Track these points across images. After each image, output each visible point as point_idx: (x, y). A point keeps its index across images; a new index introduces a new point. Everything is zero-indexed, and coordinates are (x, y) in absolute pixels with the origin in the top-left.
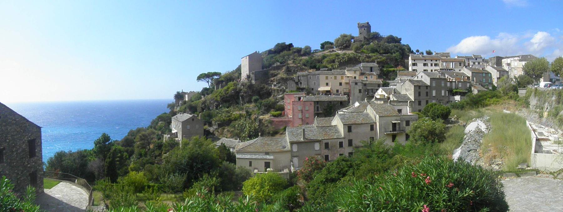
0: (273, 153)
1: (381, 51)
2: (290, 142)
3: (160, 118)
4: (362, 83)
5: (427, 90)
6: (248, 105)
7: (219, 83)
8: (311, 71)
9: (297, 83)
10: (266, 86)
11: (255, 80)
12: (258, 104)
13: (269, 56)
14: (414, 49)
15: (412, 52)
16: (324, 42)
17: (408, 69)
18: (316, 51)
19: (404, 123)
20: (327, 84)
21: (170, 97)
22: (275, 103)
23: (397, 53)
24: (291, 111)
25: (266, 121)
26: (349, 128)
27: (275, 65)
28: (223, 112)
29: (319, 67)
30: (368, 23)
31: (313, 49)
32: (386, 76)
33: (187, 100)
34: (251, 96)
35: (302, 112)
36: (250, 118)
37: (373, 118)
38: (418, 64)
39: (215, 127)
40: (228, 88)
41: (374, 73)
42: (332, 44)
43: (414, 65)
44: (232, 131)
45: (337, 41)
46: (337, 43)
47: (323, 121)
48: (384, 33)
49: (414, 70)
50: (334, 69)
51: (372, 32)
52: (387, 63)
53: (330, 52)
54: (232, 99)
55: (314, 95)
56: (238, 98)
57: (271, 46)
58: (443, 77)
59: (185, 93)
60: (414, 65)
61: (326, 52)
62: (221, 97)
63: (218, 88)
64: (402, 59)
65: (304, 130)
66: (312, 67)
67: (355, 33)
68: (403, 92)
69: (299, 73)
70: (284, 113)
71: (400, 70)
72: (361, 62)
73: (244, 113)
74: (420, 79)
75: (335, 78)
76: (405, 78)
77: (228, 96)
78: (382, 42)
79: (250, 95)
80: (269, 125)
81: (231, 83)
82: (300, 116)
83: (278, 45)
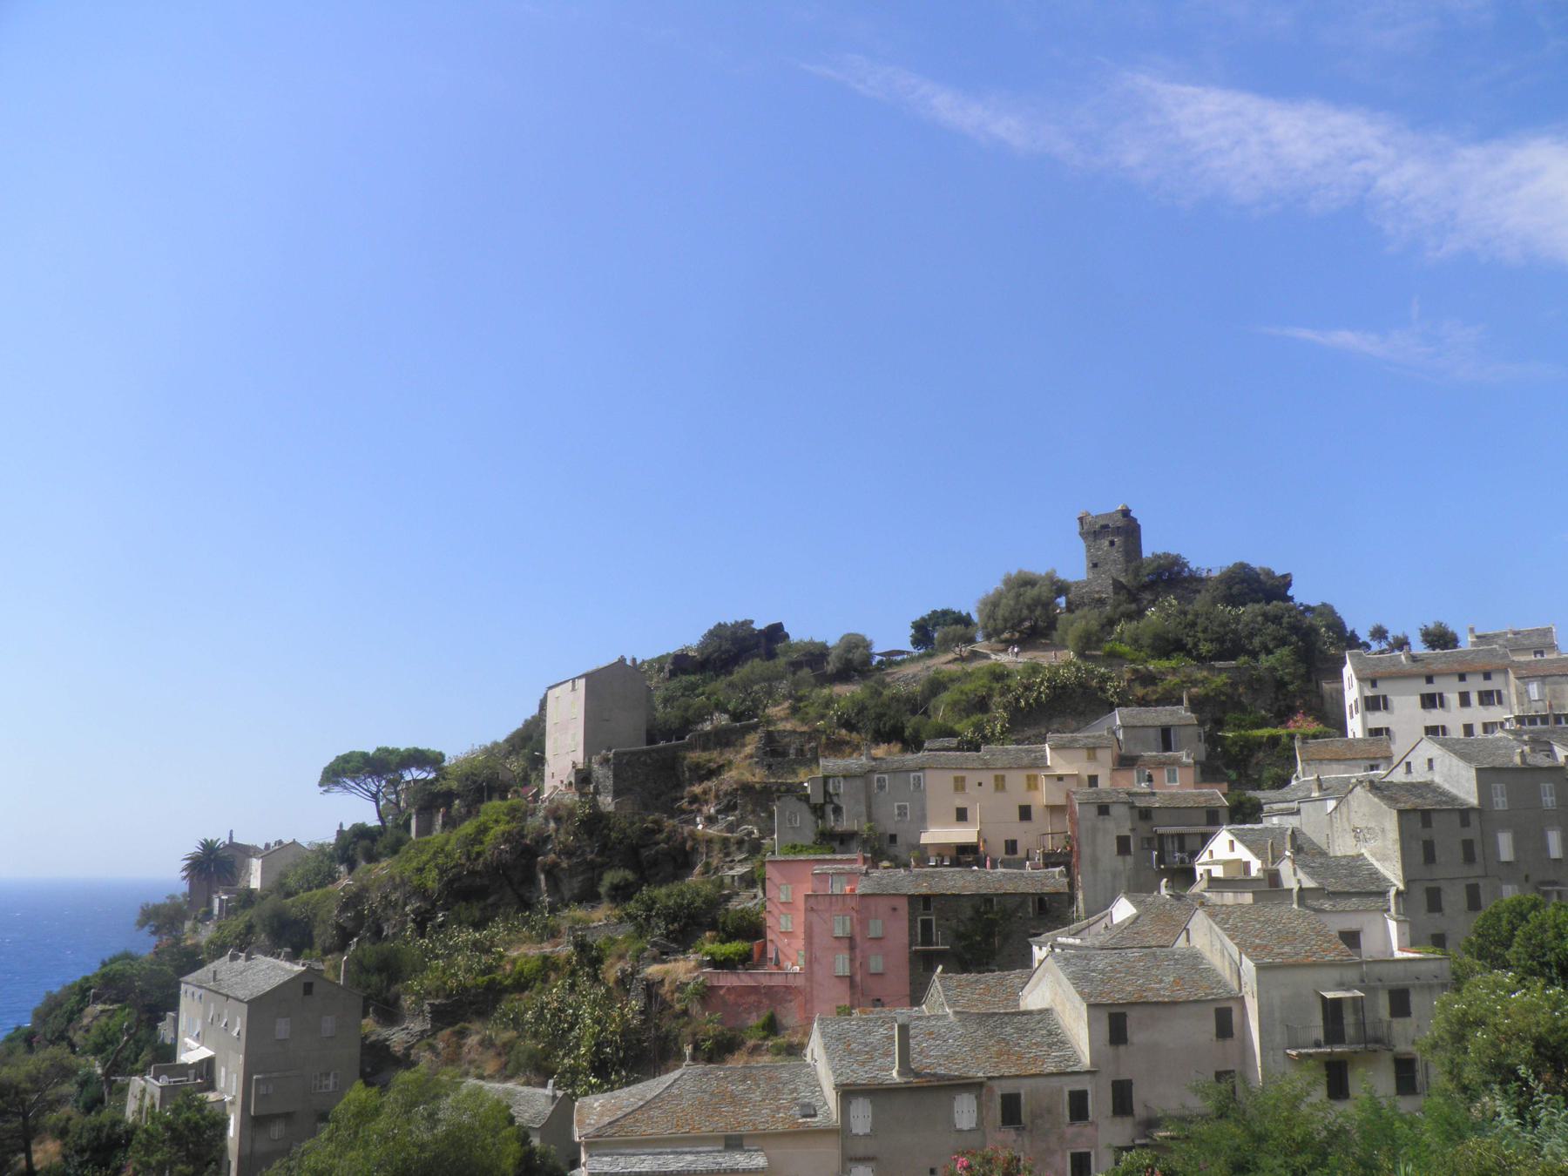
0: (763, 1139)
1: (1205, 648)
2: (837, 1086)
3: (112, 983)
4: (1132, 807)
5: (1468, 834)
6: (579, 913)
7: (432, 801)
8: (880, 751)
9: (818, 811)
10: (669, 823)
11: (617, 793)
12: (632, 907)
13: (674, 684)
14: (1359, 624)
15: (1352, 642)
16: (925, 612)
17: (1342, 728)
18: (891, 659)
19: (1383, 1002)
20: (962, 815)
21: (165, 871)
22: (716, 902)
23: (1284, 652)
24: (800, 943)
25: (681, 987)
26: (1115, 1025)
27: (708, 727)
28: (457, 949)
29: (917, 732)
30: (1126, 513)
31: (879, 647)
32: (1245, 770)
33: (255, 883)
34: (594, 871)
35: (852, 948)
36: (595, 978)
37: (1227, 973)
38: (1396, 701)
39: (416, 1026)
40: (483, 830)
41: (1184, 756)
42: (965, 621)
43: (1373, 704)
44: (508, 1047)
46: (991, 616)
47: (977, 989)
48: (1209, 557)
49: (1376, 732)
50: (987, 740)
51: (1147, 552)
52: (1239, 706)
53: (962, 659)
54: (499, 883)
55: (898, 863)
56: (531, 880)
57: (688, 636)
58: (1541, 760)
59: (247, 851)
61: (942, 663)
62: (442, 872)
63: (425, 829)
64: (1307, 678)
65: (904, 1029)
66: (881, 737)
67: (1071, 563)
68: (1343, 846)
69: (829, 764)
70: (763, 952)
71: (1305, 738)
72: (1111, 707)
73: (564, 950)
74: (1420, 775)
75: (1000, 784)
76: (1334, 773)
77: (479, 866)
78: (1200, 603)
79: (592, 866)
80: (695, 1009)
81: (496, 803)
82: (842, 965)
83: (718, 632)
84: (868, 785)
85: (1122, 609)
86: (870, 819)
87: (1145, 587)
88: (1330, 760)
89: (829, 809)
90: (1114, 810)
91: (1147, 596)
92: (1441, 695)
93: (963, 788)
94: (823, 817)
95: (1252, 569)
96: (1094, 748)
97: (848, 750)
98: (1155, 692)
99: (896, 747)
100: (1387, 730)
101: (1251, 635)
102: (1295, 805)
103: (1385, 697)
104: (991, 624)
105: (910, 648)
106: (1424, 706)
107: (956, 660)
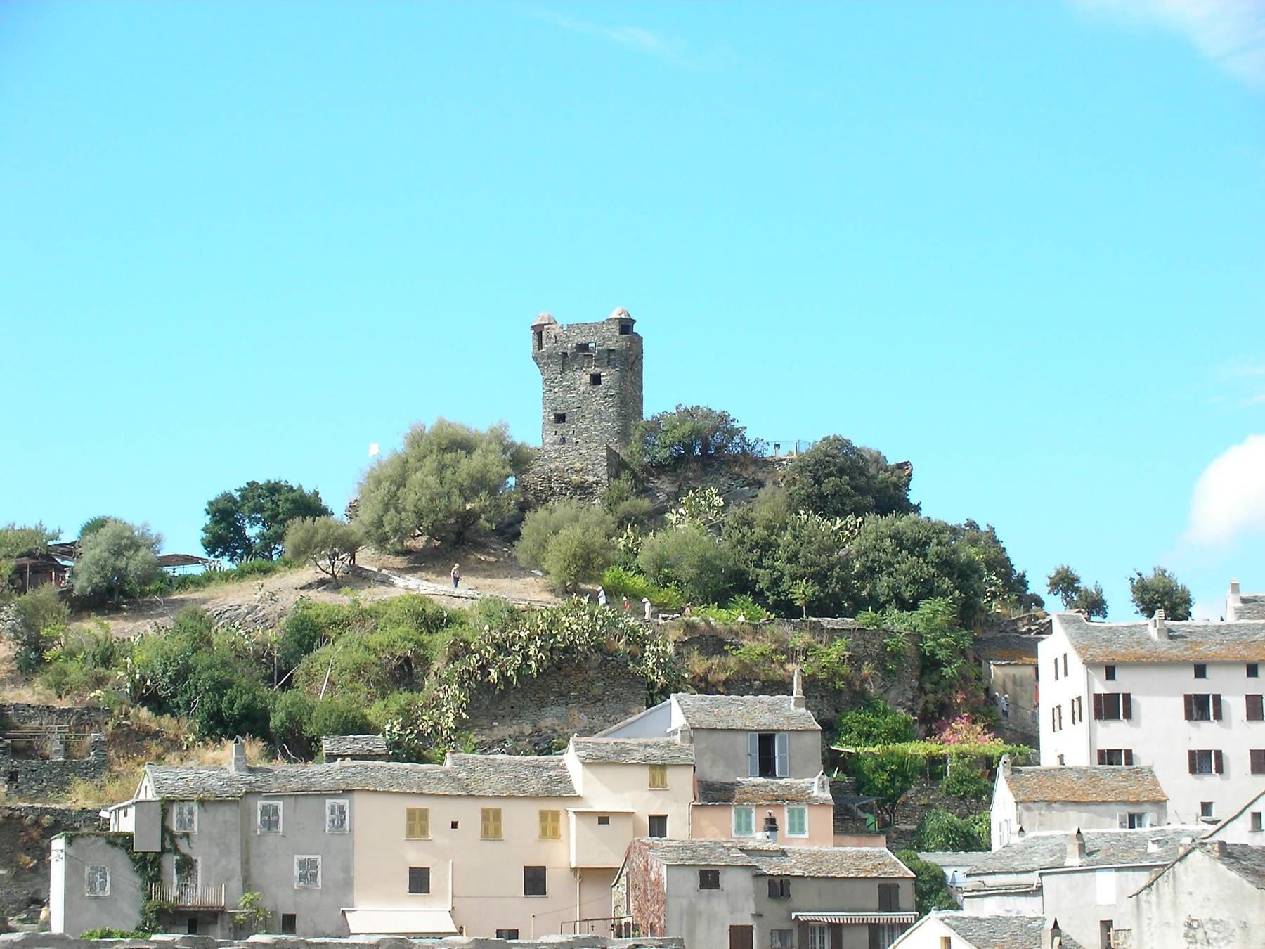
9: (148, 866)
16: (233, 484)
20: (419, 881)
30: (626, 326)
45: (392, 480)
48: (781, 425)
49: (1109, 757)
51: (650, 410)
52: (860, 699)
60: (1110, 707)
66: (221, 726)
67: (511, 405)
72: (654, 695)
75: (491, 825)
78: (767, 504)
84: (247, 816)
85: (624, 506)
86: (247, 885)
87: (659, 469)
88: (1066, 803)
89: (170, 862)
90: (726, 879)
91: (664, 486)
92: (1217, 698)
93: (424, 832)
94: (157, 879)
95: (854, 450)
96: (663, 767)
97: (156, 749)
98: (723, 667)
99: (254, 749)
100: (1129, 753)
101: (870, 572)
102: (1033, 878)
103: (1127, 698)
104: (390, 519)
105: (201, 552)
106: (1189, 716)
107: (322, 583)
